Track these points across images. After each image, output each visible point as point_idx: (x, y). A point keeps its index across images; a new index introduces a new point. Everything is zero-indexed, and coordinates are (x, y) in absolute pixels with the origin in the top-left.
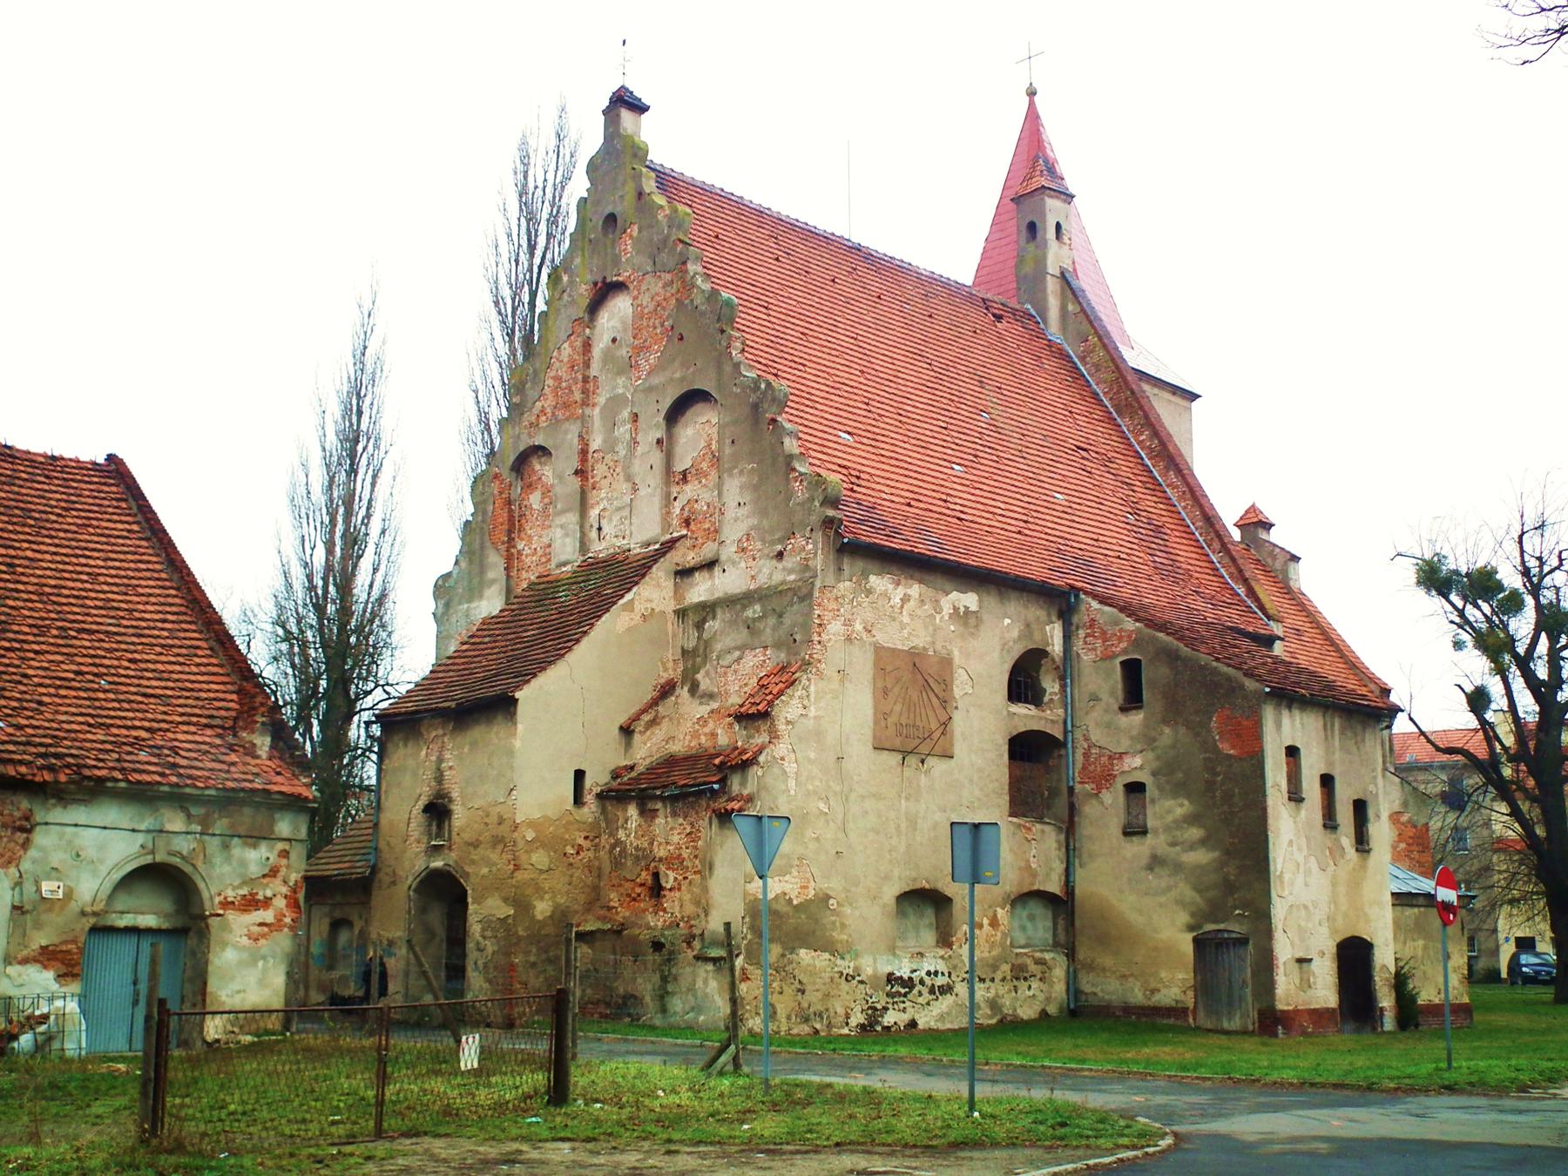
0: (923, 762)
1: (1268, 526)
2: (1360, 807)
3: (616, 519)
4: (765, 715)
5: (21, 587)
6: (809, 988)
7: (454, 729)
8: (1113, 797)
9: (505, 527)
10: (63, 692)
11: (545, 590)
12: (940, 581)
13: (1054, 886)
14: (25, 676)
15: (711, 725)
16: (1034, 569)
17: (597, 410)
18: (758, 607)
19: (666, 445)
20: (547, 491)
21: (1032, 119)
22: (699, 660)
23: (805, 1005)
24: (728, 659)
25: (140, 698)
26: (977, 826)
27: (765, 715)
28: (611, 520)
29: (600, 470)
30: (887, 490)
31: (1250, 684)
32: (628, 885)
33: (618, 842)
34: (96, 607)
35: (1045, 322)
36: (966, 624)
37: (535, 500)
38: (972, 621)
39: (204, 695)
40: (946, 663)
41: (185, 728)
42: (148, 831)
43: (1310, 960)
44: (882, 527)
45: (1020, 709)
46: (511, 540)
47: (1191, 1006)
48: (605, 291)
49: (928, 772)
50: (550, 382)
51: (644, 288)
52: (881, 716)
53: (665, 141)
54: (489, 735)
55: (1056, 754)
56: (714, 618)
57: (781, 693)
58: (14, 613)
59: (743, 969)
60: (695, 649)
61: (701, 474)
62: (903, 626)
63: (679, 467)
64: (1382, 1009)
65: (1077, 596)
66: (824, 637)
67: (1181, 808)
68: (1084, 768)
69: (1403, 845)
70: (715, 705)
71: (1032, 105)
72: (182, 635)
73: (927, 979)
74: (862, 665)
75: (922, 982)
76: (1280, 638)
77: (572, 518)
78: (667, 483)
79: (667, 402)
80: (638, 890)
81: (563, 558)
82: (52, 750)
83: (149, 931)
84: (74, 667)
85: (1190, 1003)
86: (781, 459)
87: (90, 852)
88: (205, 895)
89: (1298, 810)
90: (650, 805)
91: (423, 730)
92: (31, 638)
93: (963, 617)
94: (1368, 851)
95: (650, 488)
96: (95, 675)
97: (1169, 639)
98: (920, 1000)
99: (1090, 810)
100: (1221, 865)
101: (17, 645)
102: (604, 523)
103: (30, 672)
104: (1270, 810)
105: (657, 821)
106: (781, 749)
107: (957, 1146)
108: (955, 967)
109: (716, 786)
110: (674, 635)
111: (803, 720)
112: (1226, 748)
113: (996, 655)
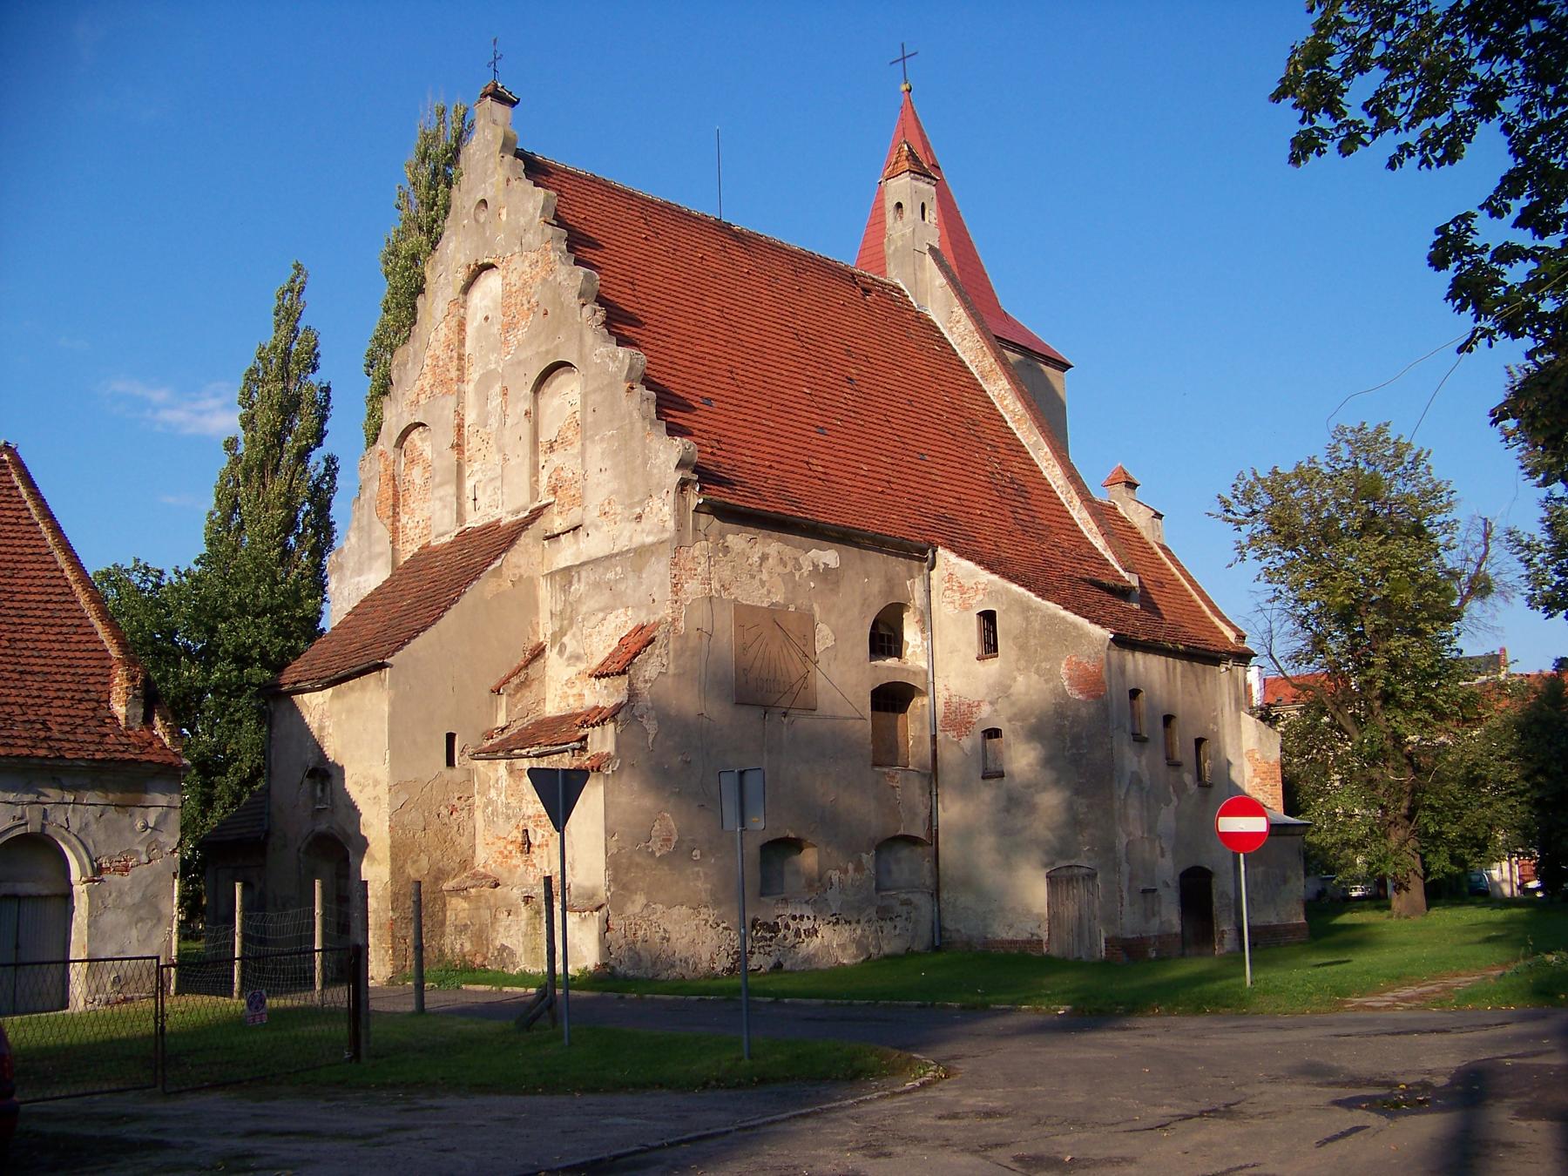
3: (489, 490)
9: (391, 502)
17: (472, 385)
19: (533, 416)
24: (594, 620)
28: (484, 491)
30: (748, 452)
32: (501, 843)
37: (417, 474)
47: (1045, 938)
50: (428, 361)
61: (565, 442)
62: (763, 583)
63: (544, 438)
69: (1258, 780)
73: (791, 923)
75: (787, 927)
77: (451, 490)
80: (510, 847)
81: (442, 530)
93: (825, 575)
100: (1070, 807)
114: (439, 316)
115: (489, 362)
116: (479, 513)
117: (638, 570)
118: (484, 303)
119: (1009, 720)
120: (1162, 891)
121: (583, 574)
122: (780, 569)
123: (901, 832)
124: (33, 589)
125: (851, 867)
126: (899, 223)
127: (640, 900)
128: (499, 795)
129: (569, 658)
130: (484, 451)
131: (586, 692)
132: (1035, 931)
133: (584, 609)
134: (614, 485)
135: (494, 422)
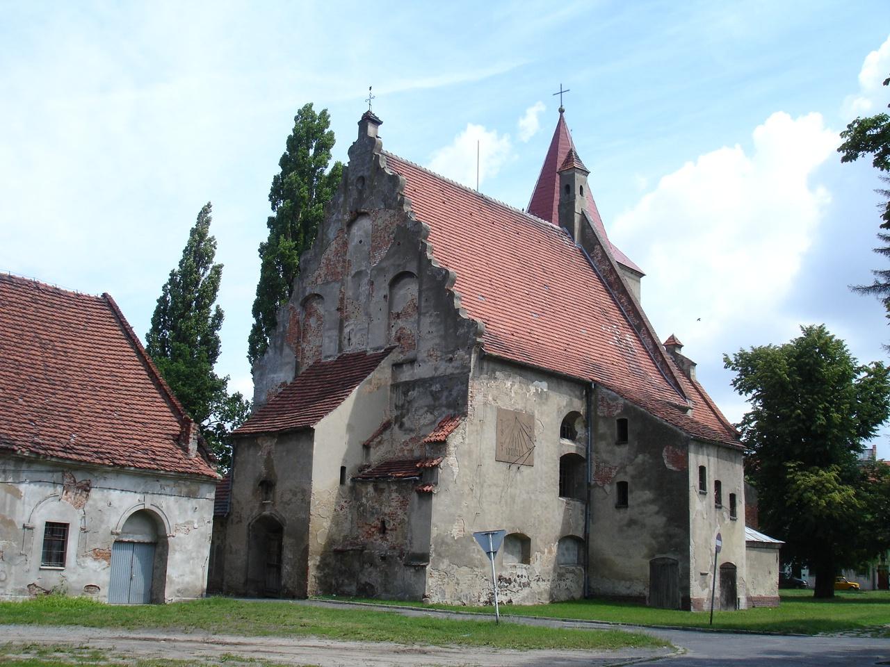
0: (519, 468)
1: (680, 346)
2: (733, 497)
3: (359, 335)
5: (71, 364)
6: (461, 582)
8: (611, 490)
10: (99, 420)
11: (319, 369)
13: (580, 534)
14: (80, 411)
15: (411, 445)
16: (575, 371)
18: (438, 386)
19: (389, 299)
20: (320, 318)
21: (561, 123)
22: (404, 411)
23: (459, 590)
25: (134, 424)
28: (355, 335)
29: (350, 308)
32: (367, 527)
33: (362, 505)
34: (107, 375)
37: (313, 322)
39: (162, 423)
40: (532, 417)
41: (156, 440)
43: (707, 574)
44: (501, 346)
45: (566, 442)
46: (298, 342)
51: (379, 216)
52: (500, 444)
56: (413, 390)
57: (452, 431)
58: (70, 377)
60: (403, 406)
67: (648, 495)
68: (596, 473)
70: (413, 435)
71: (561, 118)
72: (148, 390)
74: (491, 419)
75: (515, 581)
76: (691, 409)
77: (335, 333)
78: (389, 318)
79: (390, 276)
81: (329, 353)
82: (99, 450)
84: (102, 407)
85: (647, 593)
87: (115, 503)
90: (381, 486)
92: (79, 391)
94: (735, 520)
95: (380, 320)
96: (111, 411)
99: (597, 494)
101: (74, 395)
103: (83, 409)
107: (655, 627)
108: (531, 573)
109: (417, 478)
112: (670, 466)
113: (555, 414)
116: (352, 347)
122: (520, 391)
123: (570, 534)
124: (130, 376)
125: (546, 551)
127: (446, 561)
128: (368, 502)
130: (356, 313)
133: (416, 405)
134: (437, 341)
135: (363, 299)
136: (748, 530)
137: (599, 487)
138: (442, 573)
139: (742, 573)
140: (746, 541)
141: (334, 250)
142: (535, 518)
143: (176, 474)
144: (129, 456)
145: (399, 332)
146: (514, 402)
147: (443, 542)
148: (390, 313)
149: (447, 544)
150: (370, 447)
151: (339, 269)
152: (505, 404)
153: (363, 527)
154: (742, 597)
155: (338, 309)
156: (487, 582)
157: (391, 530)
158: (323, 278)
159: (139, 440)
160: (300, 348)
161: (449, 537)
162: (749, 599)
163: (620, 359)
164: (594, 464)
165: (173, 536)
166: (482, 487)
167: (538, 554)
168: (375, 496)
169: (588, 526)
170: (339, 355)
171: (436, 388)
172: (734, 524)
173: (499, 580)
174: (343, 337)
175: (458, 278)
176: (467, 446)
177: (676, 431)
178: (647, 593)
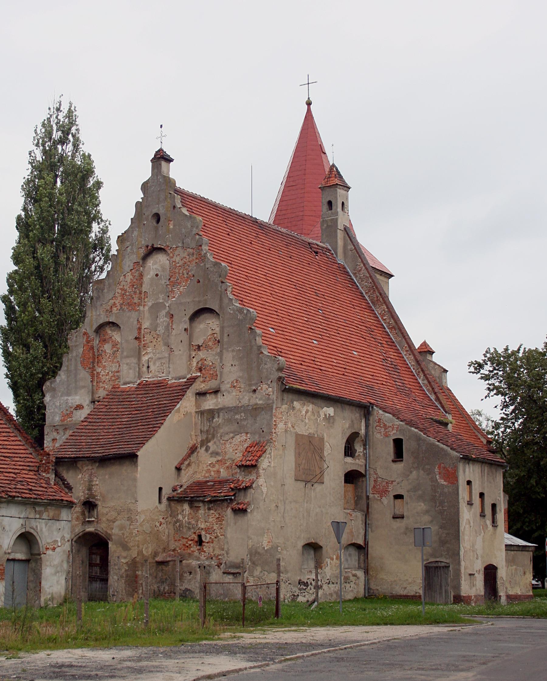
0: (313, 485)
2: (494, 506)
3: (158, 364)
4: (254, 466)
7: (98, 467)
12: (319, 402)
13: (361, 542)
16: (353, 395)
17: (147, 308)
20: (115, 345)
21: (309, 118)
22: (210, 436)
26: (423, 529)
27: (254, 466)
28: (154, 364)
29: (148, 338)
31: (455, 453)
32: (185, 540)
33: (178, 521)
35: (337, 255)
36: (329, 422)
38: (331, 421)
40: (322, 440)
42: (24, 518)
43: (474, 575)
45: (349, 460)
46: (94, 366)
48: (152, 250)
49: (314, 489)
52: (298, 465)
53: (182, 176)
54: (124, 470)
55: (361, 480)
57: (260, 456)
59: (247, 578)
61: (207, 347)
64: (500, 596)
65: (372, 407)
66: (277, 430)
68: (374, 487)
70: (220, 458)
71: (309, 111)
75: (311, 584)
78: (190, 350)
79: (191, 312)
80: (190, 542)
81: (128, 380)
83: (19, 560)
86: (255, 347)
88: (41, 545)
89: (471, 508)
90: (196, 504)
91: (79, 466)
93: (329, 419)
94: (497, 526)
95: (181, 350)
97: (416, 430)
98: (311, 592)
99: (375, 506)
102: (151, 364)
104: (460, 509)
105: (200, 512)
106: (261, 481)
109: (233, 498)
110: (196, 424)
111: (269, 468)
113: (340, 436)
114: (127, 268)
115: (159, 298)
117: (255, 417)
118: (155, 267)
119: (408, 491)
120: (476, 575)
121: (221, 414)
122: (312, 417)
123: (353, 542)
125: (335, 557)
126: (330, 212)
127: (259, 569)
128: (184, 518)
129: (212, 453)
131: (222, 470)
132: (418, 591)
133: (221, 431)
135: (161, 330)
136: (507, 536)
137: (377, 500)
138: (256, 579)
139: (502, 573)
140: (506, 545)
141: (129, 281)
142: (325, 529)
143: (49, 502)
144: (15, 488)
145: (200, 363)
146: (308, 428)
147: (257, 553)
148: (190, 345)
149: (259, 553)
150: (181, 469)
151: (136, 300)
152: (302, 430)
153: (180, 540)
154: (502, 593)
155: (136, 338)
156: (290, 585)
157: (208, 543)
158: (119, 307)
159: (14, 473)
160: (95, 372)
161: (261, 548)
162: (509, 597)
163: (388, 378)
164: (372, 479)
165: (45, 554)
166: (285, 503)
167: (329, 560)
168: (190, 513)
169: (367, 533)
170: (139, 381)
171: (241, 416)
172: (495, 530)
173: (299, 583)
174: (141, 365)
175: (258, 318)
176: (272, 469)
177: (446, 451)
178: (421, 592)
